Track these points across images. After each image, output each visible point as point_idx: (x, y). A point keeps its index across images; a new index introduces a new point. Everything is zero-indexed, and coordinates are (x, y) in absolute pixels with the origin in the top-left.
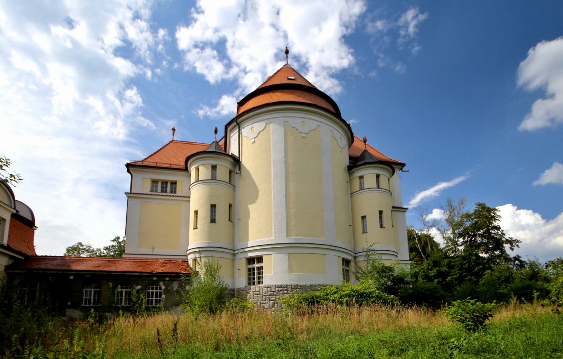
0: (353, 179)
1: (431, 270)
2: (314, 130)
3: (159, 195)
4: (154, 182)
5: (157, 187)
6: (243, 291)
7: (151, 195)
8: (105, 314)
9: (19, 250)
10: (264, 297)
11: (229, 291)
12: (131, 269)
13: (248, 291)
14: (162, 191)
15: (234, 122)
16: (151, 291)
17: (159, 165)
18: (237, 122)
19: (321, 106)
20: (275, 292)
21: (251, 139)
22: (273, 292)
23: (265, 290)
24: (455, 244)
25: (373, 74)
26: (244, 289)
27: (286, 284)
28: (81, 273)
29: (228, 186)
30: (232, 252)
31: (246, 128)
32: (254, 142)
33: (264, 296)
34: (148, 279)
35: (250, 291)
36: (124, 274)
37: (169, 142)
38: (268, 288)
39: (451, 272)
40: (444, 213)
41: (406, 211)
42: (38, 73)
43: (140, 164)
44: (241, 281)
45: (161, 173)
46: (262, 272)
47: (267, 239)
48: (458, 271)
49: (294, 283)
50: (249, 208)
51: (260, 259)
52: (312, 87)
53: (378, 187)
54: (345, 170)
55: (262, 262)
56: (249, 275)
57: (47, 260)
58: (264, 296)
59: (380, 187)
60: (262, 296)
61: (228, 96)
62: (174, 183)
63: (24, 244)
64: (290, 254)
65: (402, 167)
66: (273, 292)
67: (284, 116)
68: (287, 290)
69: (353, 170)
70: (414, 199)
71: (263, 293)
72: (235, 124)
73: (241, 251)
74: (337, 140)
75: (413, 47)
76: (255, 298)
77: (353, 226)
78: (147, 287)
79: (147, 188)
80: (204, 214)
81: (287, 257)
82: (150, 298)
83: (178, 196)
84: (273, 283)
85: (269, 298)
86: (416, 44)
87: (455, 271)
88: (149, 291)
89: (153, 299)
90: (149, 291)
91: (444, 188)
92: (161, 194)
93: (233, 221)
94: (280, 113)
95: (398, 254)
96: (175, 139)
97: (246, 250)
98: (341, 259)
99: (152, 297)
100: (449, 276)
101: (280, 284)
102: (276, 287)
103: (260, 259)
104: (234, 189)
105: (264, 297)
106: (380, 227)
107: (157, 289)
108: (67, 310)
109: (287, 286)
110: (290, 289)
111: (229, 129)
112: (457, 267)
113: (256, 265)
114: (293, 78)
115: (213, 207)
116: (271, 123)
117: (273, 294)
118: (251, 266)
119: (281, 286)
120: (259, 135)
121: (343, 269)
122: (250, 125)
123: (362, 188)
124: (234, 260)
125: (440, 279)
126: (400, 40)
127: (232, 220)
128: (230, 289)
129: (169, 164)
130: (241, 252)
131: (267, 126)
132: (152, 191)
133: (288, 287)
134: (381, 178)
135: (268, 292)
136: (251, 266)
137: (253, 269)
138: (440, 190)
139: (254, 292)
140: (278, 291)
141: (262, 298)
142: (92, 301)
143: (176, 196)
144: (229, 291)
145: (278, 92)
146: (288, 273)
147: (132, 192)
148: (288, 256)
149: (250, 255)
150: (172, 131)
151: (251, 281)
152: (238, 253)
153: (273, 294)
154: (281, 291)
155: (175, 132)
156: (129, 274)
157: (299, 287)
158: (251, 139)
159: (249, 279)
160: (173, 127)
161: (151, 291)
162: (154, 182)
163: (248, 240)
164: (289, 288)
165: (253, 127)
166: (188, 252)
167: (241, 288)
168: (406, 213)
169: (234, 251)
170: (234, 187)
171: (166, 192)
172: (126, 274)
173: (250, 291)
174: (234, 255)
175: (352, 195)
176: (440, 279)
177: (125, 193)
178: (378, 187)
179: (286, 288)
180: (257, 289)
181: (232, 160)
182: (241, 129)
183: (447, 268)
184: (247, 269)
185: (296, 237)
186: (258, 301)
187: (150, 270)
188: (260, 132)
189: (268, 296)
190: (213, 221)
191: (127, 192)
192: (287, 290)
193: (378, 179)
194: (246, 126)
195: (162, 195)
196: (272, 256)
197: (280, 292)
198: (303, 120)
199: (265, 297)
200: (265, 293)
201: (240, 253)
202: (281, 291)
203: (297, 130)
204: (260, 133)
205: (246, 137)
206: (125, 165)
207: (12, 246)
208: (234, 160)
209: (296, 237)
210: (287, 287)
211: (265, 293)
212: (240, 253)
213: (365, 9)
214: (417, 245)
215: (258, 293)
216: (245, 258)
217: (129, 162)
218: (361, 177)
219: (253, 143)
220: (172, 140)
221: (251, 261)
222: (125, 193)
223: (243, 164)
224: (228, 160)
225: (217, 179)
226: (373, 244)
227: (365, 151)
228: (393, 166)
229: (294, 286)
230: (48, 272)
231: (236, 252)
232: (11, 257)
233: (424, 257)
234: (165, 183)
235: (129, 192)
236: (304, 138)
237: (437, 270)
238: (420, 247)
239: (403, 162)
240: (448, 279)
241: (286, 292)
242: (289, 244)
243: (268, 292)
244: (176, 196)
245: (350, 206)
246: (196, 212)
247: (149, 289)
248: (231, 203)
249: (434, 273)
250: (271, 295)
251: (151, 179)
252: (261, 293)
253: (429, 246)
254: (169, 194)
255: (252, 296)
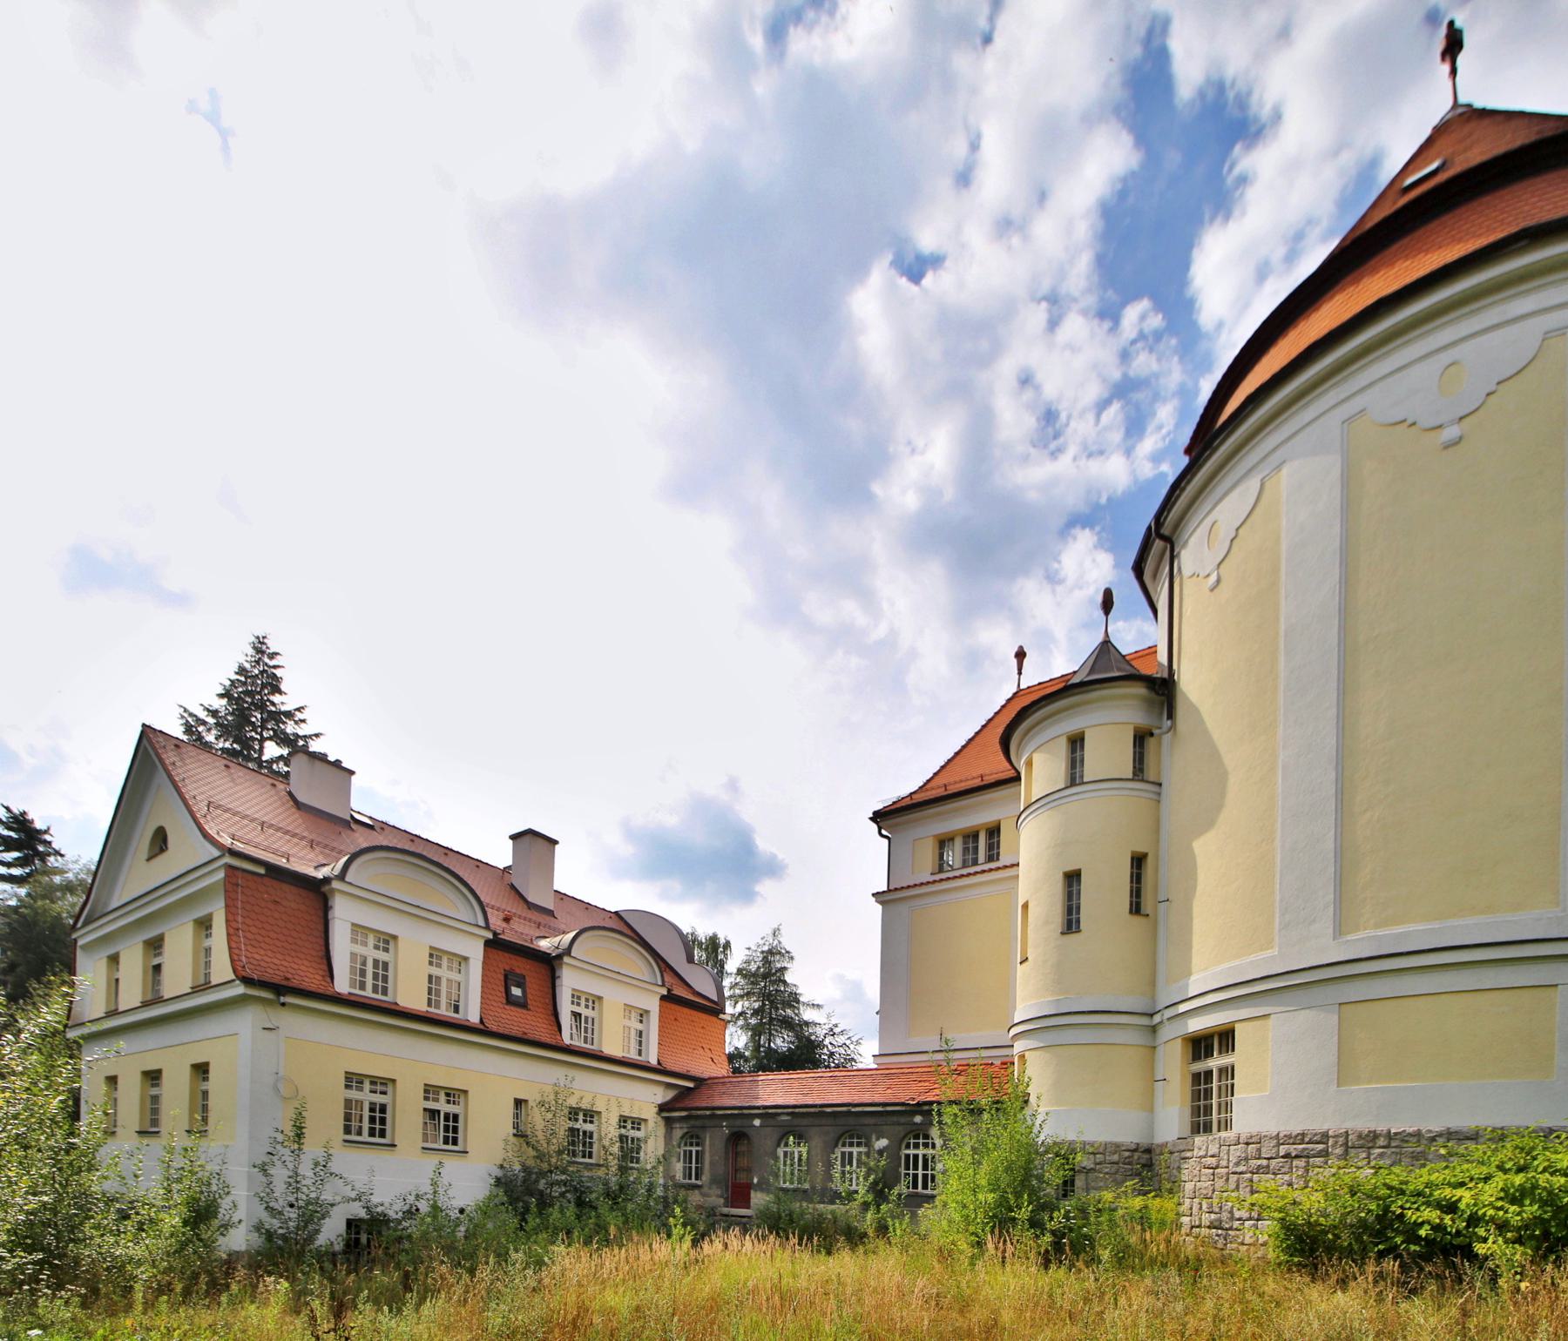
5: (976, 849)
8: (318, 1243)
9: (685, 1072)
10: (1233, 1178)
11: (1127, 1154)
12: (867, 1098)
13: (1184, 1154)
15: (1154, 540)
16: (912, 1152)
20: (1273, 1162)
22: (1268, 1159)
23: (1236, 1152)
27: (1325, 1128)
29: (1031, 817)
30: (1145, 1021)
32: (1218, 581)
34: (903, 1120)
38: (1247, 1144)
42: (861, 620)
43: (908, 801)
45: (939, 814)
46: (1233, 1085)
47: (1252, 958)
49: (1364, 1124)
50: (1197, 851)
51: (1225, 1038)
52: (1549, 131)
56: (1196, 1096)
60: (1228, 1174)
61: (32, 822)
66: (1265, 1162)
71: (1231, 1164)
72: (1158, 544)
73: (1169, 1013)
83: (1006, 867)
84: (1270, 1124)
85: (1251, 1181)
88: (907, 1152)
90: (907, 1152)
92: (965, 871)
93: (1149, 911)
94: (1327, 390)
99: (916, 1168)
102: (1279, 1140)
103: (1225, 1038)
105: (1233, 1178)
106: (1131, 912)
111: (1147, 577)
113: (1215, 1063)
115: (1072, 878)
116: (1284, 462)
117: (1268, 1166)
118: (1200, 1066)
119: (1301, 1138)
120: (1235, 542)
128: (1134, 1147)
130: (1169, 1019)
133: (1331, 1142)
135: (1246, 1159)
136: (1200, 1066)
137: (1209, 1074)
139: (1201, 1157)
140: (1287, 1156)
141: (1227, 1180)
143: (999, 868)
144: (1127, 1154)
148: (1336, 1017)
149: (1196, 1025)
150: (1014, 662)
151: (1201, 1124)
152: (1161, 1022)
153: (1268, 1166)
154: (1297, 1157)
155: (1026, 662)
157: (1381, 1142)
159: (1196, 1111)
161: (912, 1152)
164: (1333, 1146)
166: (1014, 1031)
169: (1151, 1015)
171: (975, 862)
173: (1189, 1154)
174: (1154, 1029)
179: (1321, 1147)
180: (1213, 1149)
181: (1140, 690)
186: (1214, 1191)
187: (908, 1098)
188: (1237, 529)
189: (1249, 1175)
190: (1071, 924)
192: (1325, 1154)
195: (969, 875)
196: (1271, 1022)
197: (1295, 1163)
198: (1446, 358)
200: (1237, 1164)
202: (1297, 1157)
204: (1241, 531)
206: (871, 819)
207: (670, 1065)
208: (1148, 688)
211: (1237, 1164)
212: (1167, 1023)
215: (1213, 1161)
217: (879, 807)
221: (1200, 1045)
222: (873, 895)
223: (1183, 693)
224: (1124, 697)
229: (1360, 1136)
231: (1157, 1019)
232: (669, 1086)
234: (971, 836)
236: (1457, 442)
241: (1318, 1161)
242: (1318, 971)
243: (1246, 1159)
246: (1025, 906)
250: (1264, 1170)
251: (934, 836)
252: (1224, 1163)
254: (986, 867)
255: (1196, 1172)
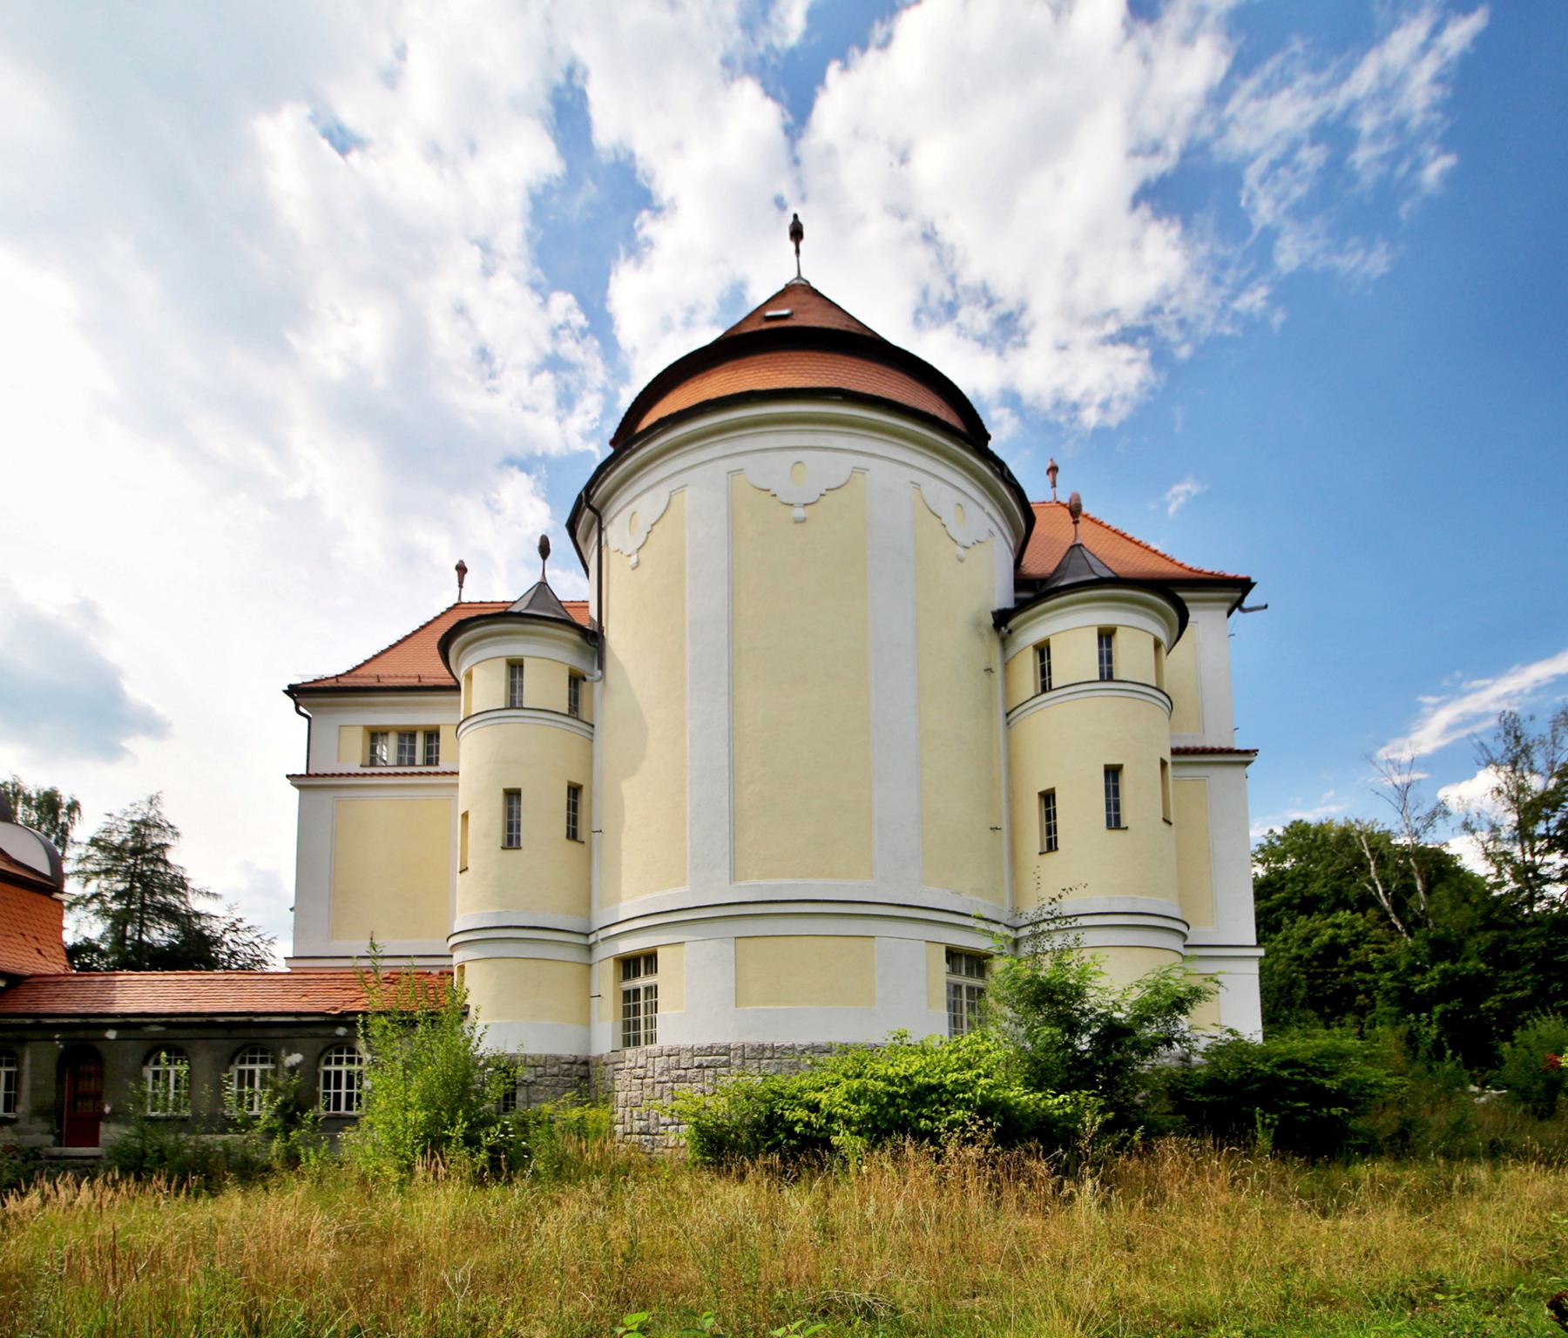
0: (1014, 656)
1: (1423, 971)
2: (838, 488)
3: (421, 774)
4: (375, 735)
6: (606, 1065)
7: (365, 775)
10: (658, 1087)
11: (566, 1066)
14: (400, 763)
16: (333, 1068)
17: (386, 682)
18: (592, 508)
19: (906, 402)
21: (630, 556)
23: (661, 1063)
24: (1530, 875)
25: (1254, 299)
26: (608, 1058)
28: (133, 1020)
30: (581, 940)
31: (616, 520)
32: (638, 563)
33: (659, 1082)
34: (322, 1032)
35: (620, 1066)
36: (40, 1022)
37: (444, 610)
38: (669, 1056)
39: (1504, 978)
40: (1498, 771)
41: (1247, 763)
43: (333, 683)
44: (604, 1037)
47: (670, 891)
48: (1529, 974)
49: (754, 1039)
53: (1107, 675)
54: (978, 625)
55: (656, 972)
57: (66, 985)
58: (659, 1082)
59: (1115, 678)
60: (654, 1083)
62: (432, 735)
63: (25, 942)
64: (738, 940)
65: (1239, 595)
66: (683, 1072)
67: (728, 452)
68: (728, 1064)
69: (1011, 624)
70: (1421, 729)
71: (656, 1075)
72: (587, 513)
73: (603, 934)
74: (940, 518)
75: (1418, 166)
76: (633, 1088)
77: (1007, 831)
78: (322, 1054)
79: (352, 757)
80: (487, 818)
81: (729, 949)
82: (332, 1091)
85: (673, 1089)
86: (1432, 151)
87: (1520, 977)
88: (242, 1067)
89: (340, 1093)
90: (242, 1067)
91: (1537, 681)
92: (424, 769)
93: (584, 839)
95: (1189, 928)
96: (464, 599)
97: (612, 933)
98: (943, 949)
99: (338, 1086)
100: (1495, 993)
101: (706, 1043)
104: (592, 734)
105: (658, 1087)
107: (351, 1061)
108: (102, 1127)
109: (727, 1050)
110: (738, 1062)
112: (1527, 962)
113: (641, 982)
114: (785, 312)
115: (512, 795)
116: (686, 485)
117: (686, 1076)
118: (630, 985)
119: (710, 1050)
121: (948, 983)
122: (624, 512)
123: (1046, 687)
124: (590, 965)
125: (1455, 1004)
126: (1362, 155)
127: (583, 833)
128: (572, 1059)
129: (415, 677)
130: (603, 940)
131: (675, 498)
132: (400, 763)
133: (732, 1054)
134: (1120, 642)
135: (668, 1070)
136: (630, 985)
137: (637, 991)
138: (1521, 692)
140: (699, 1067)
141: (653, 1089)
142: (171, 1104)
143: (437, 774)
144: (566, 1066)
145: (719, 373)
146: (733, 1007)
147: (310, 772)
149: (628, 946)
152: (596, 942)
154: (707, 1067)
155: (467, 576)
156: (66, 1021)
157: (768, 1054)
158: (630, 556)
160: (457, 562)
161: (333, 1068)
162: (375, 735)
163: (619, 900)
165: (634, 513)
167: (602, 1055)
168: (1249, 769)
169: (587, 935)
170: (589, 729)
171: (412, 763)
172: (256, 1020)
174: (589, 948)
175: (1011, 716)
176: (1455, 1004)
177: (288, 776)
178: (1107, 675)
179: (725, 1058)
180: (641, 1061)
182: (605, 529)
183: (1488, 964)
184: (621, 995)
185: (762, 882)
186: (642, 1099)
187: (328, 1007)
188: (653, 525)
190: (512, 840)
191: (291, 773)
192: (728, 1064)
193: (1109, 645)
194: (616, 515)
197: (707, 1072)
198: (798, 455)
199: (660, 1085)
200: (661, 1074)
201: (601, 943)
202: (707, 1067)
203: (775, 495)
205: (618, 551)
206: (285, 692)
209: (762, 882)
210: (728, 1055)
211: (661, 1074)
212: (601, 943)
213: (1223, 64)
214: (1375, 886)
216: (612, 960)
218: (1043, 650)
219: (633, 569)
220: (456, 601)
221: (631, 965)
225: (524, 706)
226: (1064, 893)
227: (1076, 547)
228: (1180, 594)
229: (753, 1050)
230: (48, 1021)
231: (592, 939)
233: (1399, 926)
234: (407, 735)
235: (304, 773)
236: (800, 521)
237: (1445, 971)
238: (1385, 893)
239: (1242, 574)
240: (1489, 1003)
241: (723, 1070)
243: (668, 1070)
244: (437, 774)
245: (1000, 762)
247: (328, 1062)
248: (577, 780)
249: (1433, 984)
250: (678, 1079)
251: (366, 727)
253: (1419, 889)
